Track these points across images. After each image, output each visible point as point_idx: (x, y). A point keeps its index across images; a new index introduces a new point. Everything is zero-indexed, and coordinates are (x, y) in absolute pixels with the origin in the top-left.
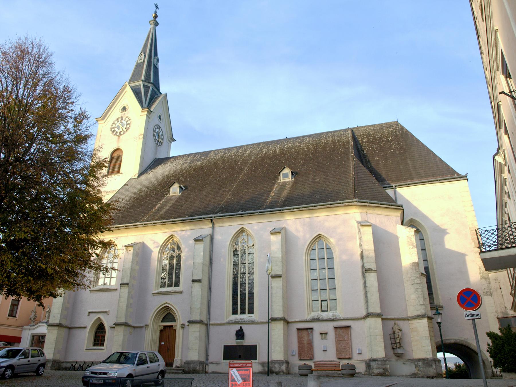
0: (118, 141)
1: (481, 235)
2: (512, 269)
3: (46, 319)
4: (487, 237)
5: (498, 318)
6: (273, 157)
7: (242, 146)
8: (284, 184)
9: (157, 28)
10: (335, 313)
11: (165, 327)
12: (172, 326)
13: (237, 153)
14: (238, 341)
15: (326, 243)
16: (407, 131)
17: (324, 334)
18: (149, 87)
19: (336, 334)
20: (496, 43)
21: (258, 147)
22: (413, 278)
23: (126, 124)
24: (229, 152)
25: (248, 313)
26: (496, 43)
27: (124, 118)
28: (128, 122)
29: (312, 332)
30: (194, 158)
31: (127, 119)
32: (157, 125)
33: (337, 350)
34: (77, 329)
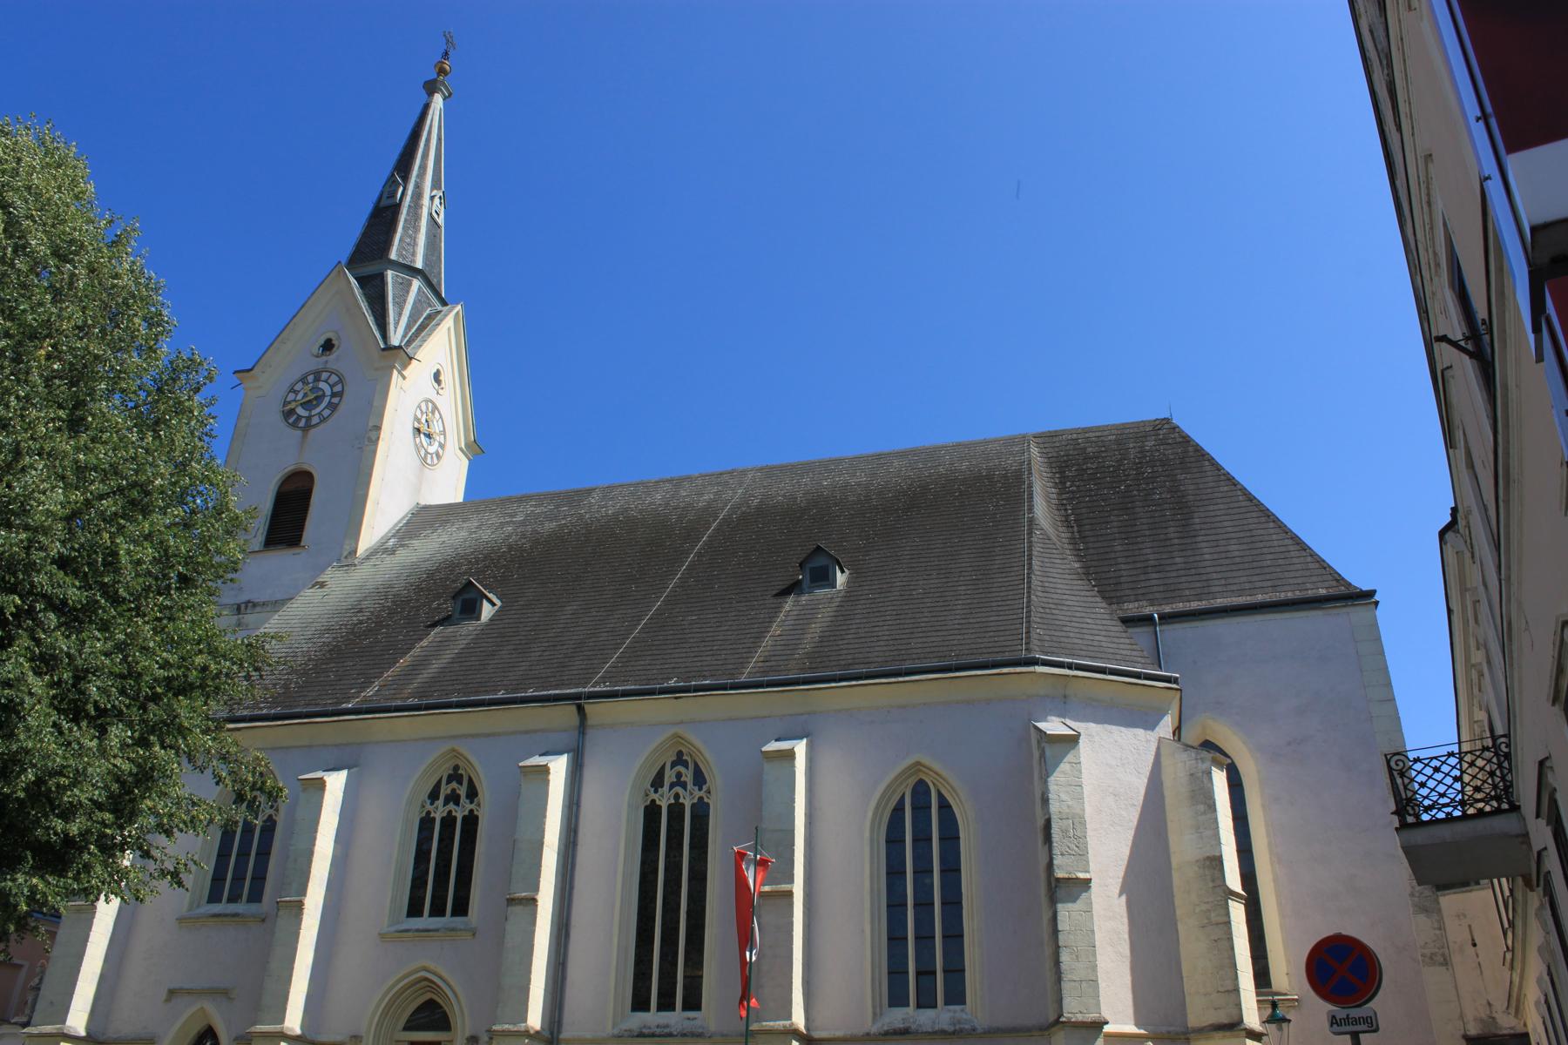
1: (1402, 775)
2: (1504, 880)
3: (27, 1011)
4: (1439, 776)
5: (1467, 1038)
10: (958, 1015)
15: (940, 795)
20: (1428, 195)
22: (1204, 907)
23: (328, 392)
26: (1428, 195)
27: (324, 376)
28: (338, 388)
31: (334, 379)
32: (427, 401)
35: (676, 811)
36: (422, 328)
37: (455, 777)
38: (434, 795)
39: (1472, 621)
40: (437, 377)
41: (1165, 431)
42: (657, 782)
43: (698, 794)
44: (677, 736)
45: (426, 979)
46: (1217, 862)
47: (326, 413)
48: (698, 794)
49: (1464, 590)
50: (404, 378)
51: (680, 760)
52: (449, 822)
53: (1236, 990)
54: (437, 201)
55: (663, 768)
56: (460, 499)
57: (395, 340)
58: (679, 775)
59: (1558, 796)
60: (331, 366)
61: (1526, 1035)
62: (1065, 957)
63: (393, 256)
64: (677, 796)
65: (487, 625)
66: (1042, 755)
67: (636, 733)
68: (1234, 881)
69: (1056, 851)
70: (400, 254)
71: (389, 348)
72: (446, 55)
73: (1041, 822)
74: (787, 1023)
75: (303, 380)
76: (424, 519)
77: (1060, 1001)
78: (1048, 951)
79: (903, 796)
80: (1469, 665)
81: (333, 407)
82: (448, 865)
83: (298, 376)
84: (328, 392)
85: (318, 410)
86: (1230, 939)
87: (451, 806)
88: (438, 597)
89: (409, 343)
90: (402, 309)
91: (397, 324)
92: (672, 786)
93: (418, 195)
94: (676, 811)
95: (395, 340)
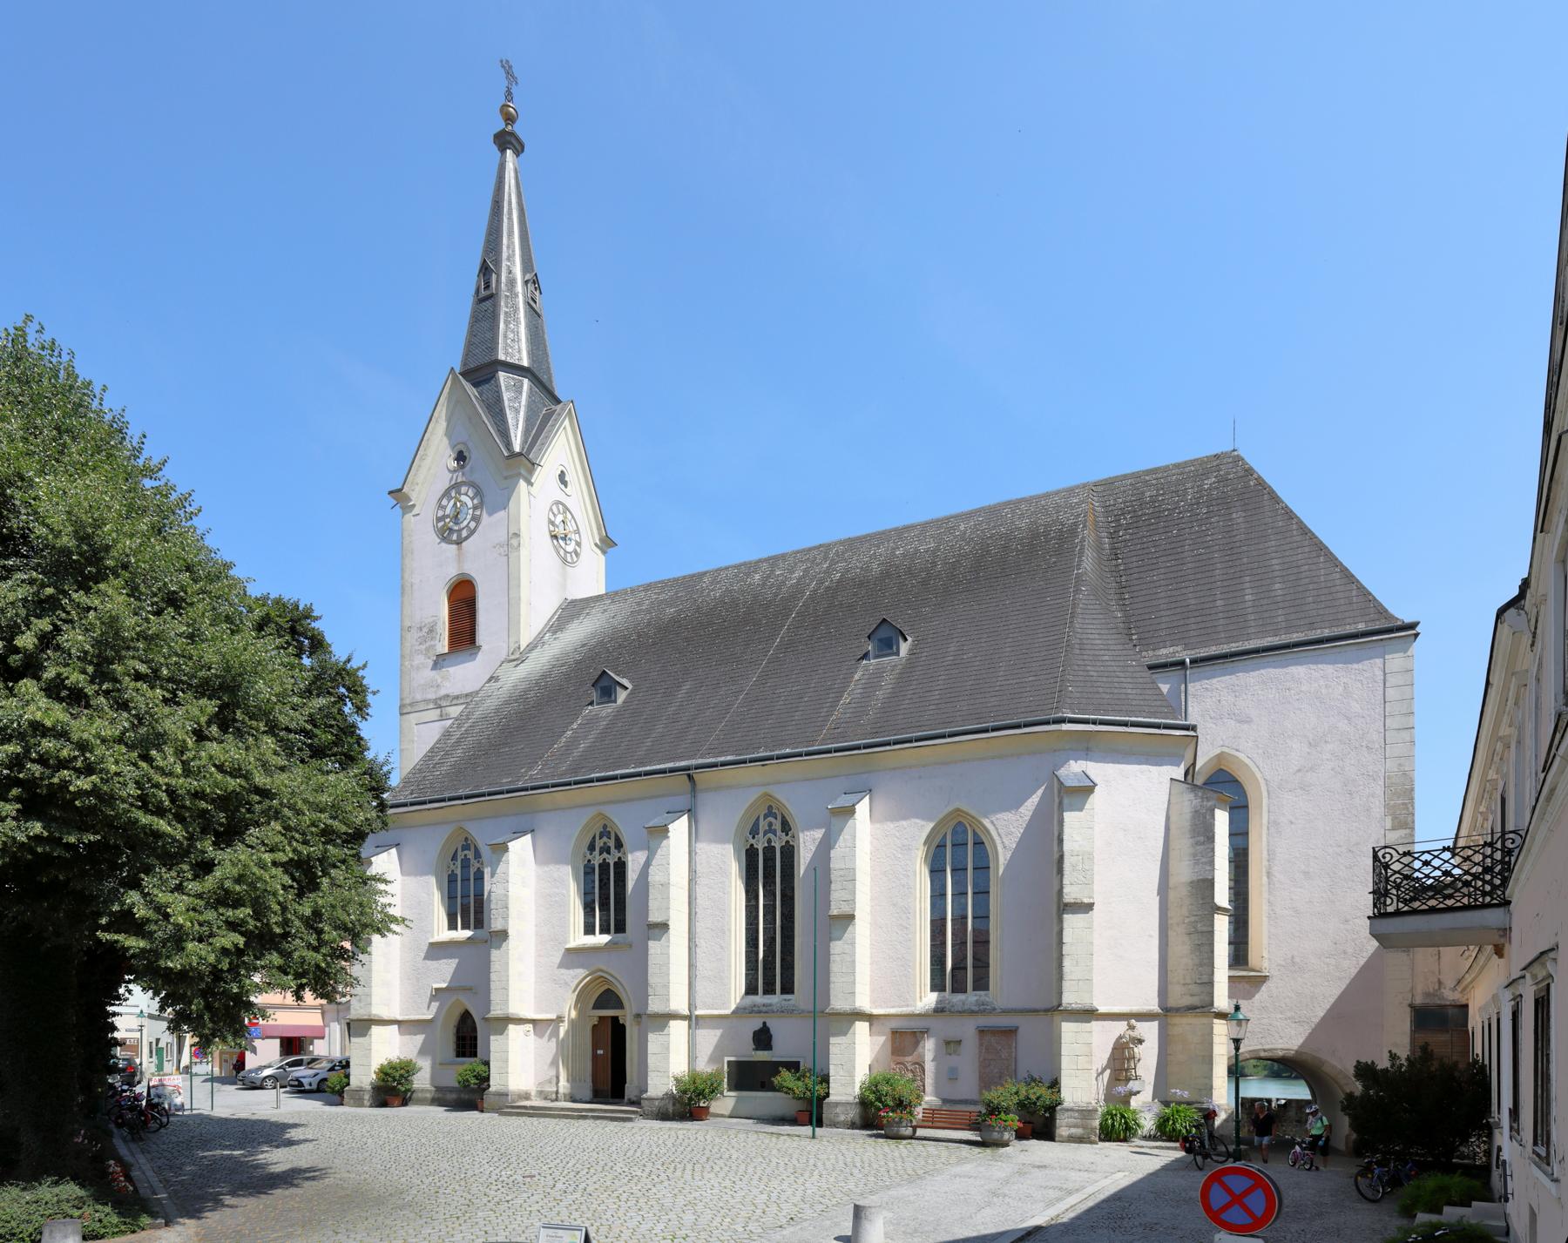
0: (460, 558)
6: (861, 584)
7: (783, 557)
13: (769, 577)
15: (975, 833)
16: (1261, 482)
20: (1256, 651)
21: (825, 559)
24: (748, 575)
30: (661, 597)
32: (558, 503)
33: (981, 1078)
35: (770, 850)
37: (605, 833)
38: (592, 848)
39: (1511, 702)
41: (1232, 461)
42: (754, 832)
43: (785, 838)
46: (1209, 884)
47: (473, 525)
48: (785, 838)
49: (1511, 673)
51: (770, 813)
53: (1211, 983)
56: (602, 591)
57: (517, 449)
58: (770, 824)
59: (1553, 987)
61: (1466, 1006)
62: (1067, 963)
64: (769, 841)
66: (1061, 803)
67: (735, 795)
68: (1222, 896)
69: (1066, 881)
71: (513, 455)
72: (509, 95)
73: (1056, 856)
76: (572, 610)
77: (1060, 994)
78: (1055, 955)
80: (1495, 737)
86: (1212, 945)
87: (605, 855)
89: (530, 450)
92: (765, 833)
94: (770, 850)
95: (517, 449)
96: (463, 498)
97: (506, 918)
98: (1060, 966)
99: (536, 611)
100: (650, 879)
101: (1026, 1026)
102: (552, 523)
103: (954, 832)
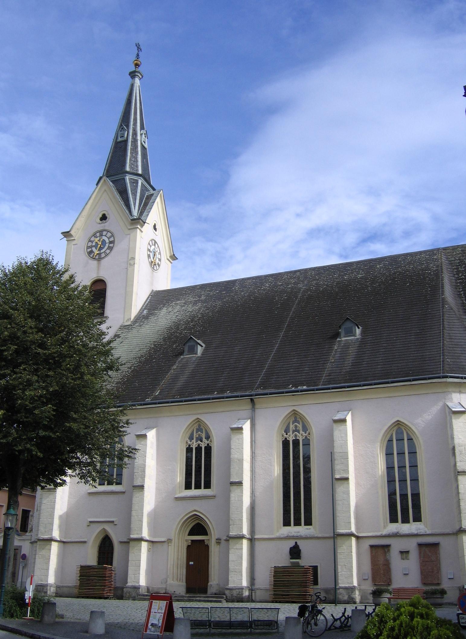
8: (347, 345)
9: (133, 69)
11: (193, 541)
12: (203, 541)
14: (292, 560)
15: (408, 434)
17: (404, 553)
18: (137, 182)
19: (420, 553)
25: (305, 525)
27: (104, 233)
28: (112, 239)
29: (389, 551)
31: (109, 235)
34: (71, 545)
36: (146, 205)
38: (191, 438)
40: (155, 228)
44: (294, 410)
45: (196, 515)
47: (108, 251)
50: (142, 232)
52: (199, 449)
54: (143, 136)
55: (289, 424)
58: (296, 426)
60: (106, 228)
63: (128, 169)
64: (296, 436)
65: (200, 358)
69: (458, 459)
70: (131, 167)
74: (350, 531)
75: (94, 235)
76: (159, 300)
79: (392, 435)
81: (111, 249)
82: (199, 467)
83: (92, 233)
84: (107, 241)
85: (103, 250)
88: (175, 342)
90: (136, 196)
91: (135, 204)
92: (293, 432)
93: (135, 134)
94: (296, 443)
96: (104, 238)
97: (143, 477)
98: (459, 506)
99: (139, 299)
100: (232, 456)
101: (445, 544)
102: (149, 250)
103: (397, 433)
